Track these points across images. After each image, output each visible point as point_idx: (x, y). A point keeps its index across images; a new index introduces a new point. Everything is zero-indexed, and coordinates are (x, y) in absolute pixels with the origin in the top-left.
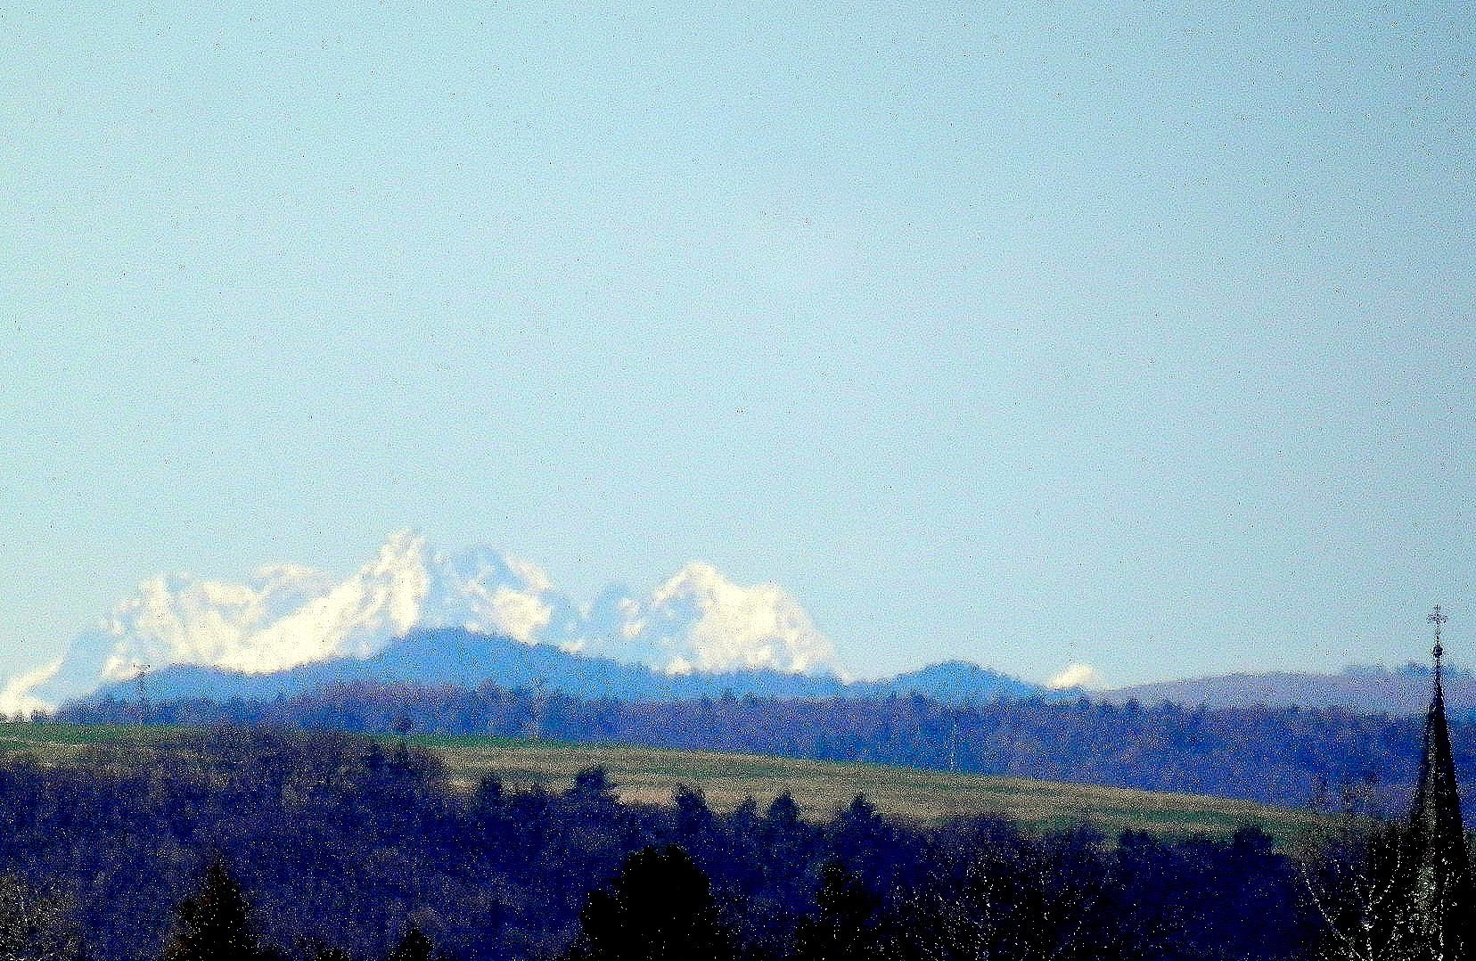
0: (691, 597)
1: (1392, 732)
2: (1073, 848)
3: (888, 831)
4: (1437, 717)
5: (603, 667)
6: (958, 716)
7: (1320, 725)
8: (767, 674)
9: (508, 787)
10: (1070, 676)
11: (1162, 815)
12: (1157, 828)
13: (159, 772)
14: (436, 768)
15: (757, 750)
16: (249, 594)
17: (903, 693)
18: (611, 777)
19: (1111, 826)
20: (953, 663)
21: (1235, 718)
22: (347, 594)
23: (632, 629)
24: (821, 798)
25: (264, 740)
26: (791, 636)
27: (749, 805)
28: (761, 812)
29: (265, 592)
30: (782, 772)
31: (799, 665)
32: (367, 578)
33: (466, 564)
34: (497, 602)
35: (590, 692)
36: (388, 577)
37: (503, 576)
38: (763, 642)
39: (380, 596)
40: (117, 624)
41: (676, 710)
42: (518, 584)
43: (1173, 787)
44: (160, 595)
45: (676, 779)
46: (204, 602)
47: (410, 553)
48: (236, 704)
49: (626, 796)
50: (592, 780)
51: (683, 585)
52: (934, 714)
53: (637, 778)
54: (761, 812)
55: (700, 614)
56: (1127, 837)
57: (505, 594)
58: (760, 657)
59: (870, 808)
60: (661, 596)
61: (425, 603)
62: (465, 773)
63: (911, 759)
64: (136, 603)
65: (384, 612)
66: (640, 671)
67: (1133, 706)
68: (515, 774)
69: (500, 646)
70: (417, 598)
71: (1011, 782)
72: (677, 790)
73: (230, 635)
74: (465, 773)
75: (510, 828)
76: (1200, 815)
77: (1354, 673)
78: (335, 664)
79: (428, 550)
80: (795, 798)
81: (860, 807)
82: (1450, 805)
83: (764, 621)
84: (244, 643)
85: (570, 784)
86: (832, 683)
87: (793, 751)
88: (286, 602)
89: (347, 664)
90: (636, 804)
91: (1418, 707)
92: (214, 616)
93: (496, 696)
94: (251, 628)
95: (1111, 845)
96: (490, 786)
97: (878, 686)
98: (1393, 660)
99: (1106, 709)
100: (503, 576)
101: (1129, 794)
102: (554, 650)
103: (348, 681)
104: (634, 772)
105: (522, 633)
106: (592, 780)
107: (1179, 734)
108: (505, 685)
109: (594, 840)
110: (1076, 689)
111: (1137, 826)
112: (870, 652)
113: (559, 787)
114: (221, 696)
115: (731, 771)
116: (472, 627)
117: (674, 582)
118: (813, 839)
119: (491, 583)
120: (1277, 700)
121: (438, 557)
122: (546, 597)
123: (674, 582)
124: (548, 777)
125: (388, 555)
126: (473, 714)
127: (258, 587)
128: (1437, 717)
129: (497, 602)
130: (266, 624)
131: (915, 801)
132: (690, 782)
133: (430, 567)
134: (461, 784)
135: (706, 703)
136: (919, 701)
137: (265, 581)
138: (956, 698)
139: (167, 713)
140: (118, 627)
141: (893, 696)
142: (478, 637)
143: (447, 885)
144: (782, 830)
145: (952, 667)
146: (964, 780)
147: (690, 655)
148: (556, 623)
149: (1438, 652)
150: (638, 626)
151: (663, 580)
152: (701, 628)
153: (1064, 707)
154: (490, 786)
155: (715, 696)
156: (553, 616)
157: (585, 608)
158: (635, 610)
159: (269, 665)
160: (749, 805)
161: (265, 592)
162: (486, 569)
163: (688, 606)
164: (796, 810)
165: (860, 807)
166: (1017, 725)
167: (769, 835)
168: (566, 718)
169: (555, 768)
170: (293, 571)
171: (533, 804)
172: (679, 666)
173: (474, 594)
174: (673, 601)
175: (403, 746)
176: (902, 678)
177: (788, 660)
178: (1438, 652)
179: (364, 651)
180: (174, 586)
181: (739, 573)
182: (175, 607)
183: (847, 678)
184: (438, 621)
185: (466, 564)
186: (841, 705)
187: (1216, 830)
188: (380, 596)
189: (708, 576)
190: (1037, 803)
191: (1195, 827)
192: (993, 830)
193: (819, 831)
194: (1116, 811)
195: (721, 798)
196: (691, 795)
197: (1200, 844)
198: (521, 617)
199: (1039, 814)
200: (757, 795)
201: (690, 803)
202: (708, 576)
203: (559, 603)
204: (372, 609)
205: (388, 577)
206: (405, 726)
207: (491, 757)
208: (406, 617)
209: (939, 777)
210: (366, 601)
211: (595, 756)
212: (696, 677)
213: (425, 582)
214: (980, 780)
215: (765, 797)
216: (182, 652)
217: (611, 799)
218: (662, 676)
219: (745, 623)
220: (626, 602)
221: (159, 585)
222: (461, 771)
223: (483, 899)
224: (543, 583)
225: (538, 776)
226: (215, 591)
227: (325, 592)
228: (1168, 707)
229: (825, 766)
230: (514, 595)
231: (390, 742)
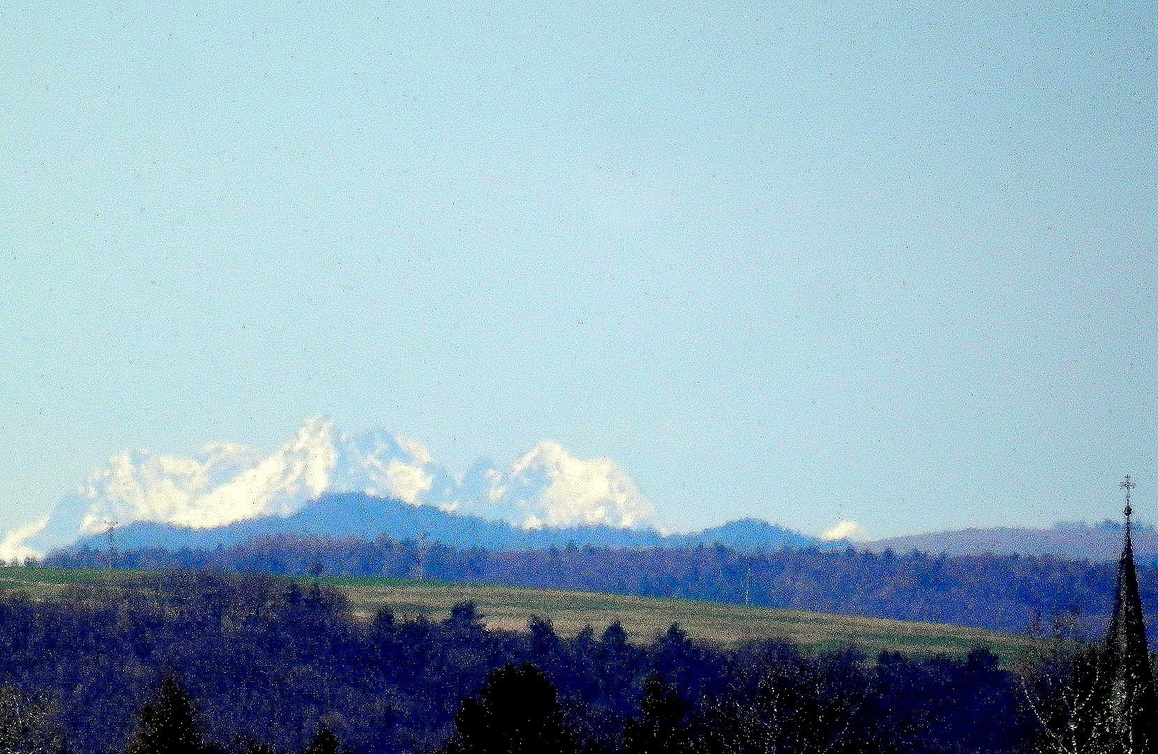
0: (542, 469)
1: (1092, 574)
2: (842, 665)
3: (696, 652)
4: (1127, 562)
5: (473, 524)
6: (752, 562)
7: (1036, 569)
8: (602, 529)
9: (399, 617)
10: (839, 530)
11: (912, 639)
12: (908, 649)
13: (124, 606)
14: (342, 603)
15: (594, 588)
16: (195, 466)
17: (709, 544)
18: (479, 610)
19: (871, 648)
20: (748, 520)
21: (969, 563)
22: (272, 466)
23: (496, 493)
24: (644, 626)
25: (207, 581)
26: (621, 499)
27: (588, 631)
28: (597, 637)
29: (208, 465)
30: (614, 606)
31: (627, 522)
32: (288, 453)
33: (366, 443)
34: (390, 472)
35: (463, 543)
36: (304, 453)
37: (395, 452)
38: (599, 504)
39: (298, 467)
40: (92, 490)
41: (531, 557)
42: (407, 458)
43: (920, 617)
44: (125, 467)
45: (531, 611)
46: (160, 472)
47: (322, 434)
48: (185, 552)
49: (491, 625)
50: (465, 612)
51: (536, 459)
52: (733, 560)
53: (500, 610)
54: (597, 637)
55: (549, 482)
56: (884, 657)
57: (397, 466)
58: (597, 516)
59: (683, 634)
60: (519, 467)
61: (334, 473)
62: (365, 607)
63: (715, 595)
64: (107, 473)
65: (301, 480)
66: (502, 527)
67: (889, 554)
68: (404, 607)
69: (392, 507)
70: (327, 469)
71: (793, 613)
72: (531, 620)
73: (181, 498)
74: (365, 607)
75: (400, 650)
76: (941, 640)
77: (1062, 528)
78: (262, 521)
79: (336, 432)
80: (624, 626)
81: (675, 633)
82: (1137, 632)
83: (599, 488)
84: (191, 504)
85: (447, 615)
86: (653, 536)
87: (622, 589)
88: (224, 473)
89: (272, 521)
90: (499, 631)
91: (1113, 554)
92: (168, 483)
93: (389, 546)
94: (197, 493)
95: (872, 663)
96: (385, 617)
97: (689, 538)
98: (1093, 518)
99: (868, 556)
100: (395, 452)
101: (886, 623)
102: (435, 510)
103: (273, 534)
104: (497, 606)
105: (410, 497)
106: (465, 612)
107: (925, 576)
108: (397, 538)
109: (466, 659)
110: (844, 541)
111: (892, 648)
112: (682, 512)
113: (438, 618)
114: (173, 546)
115: (573, 605)
116: (371, 492)
117: (529, 457)
118: (638, 658)
119: (385, 458)
120: (1002, 550)
121: (343, 437)
122: (429, 468)
123: (529, 457)
124: (430, 609)
125: (304, 435)
126: (371, 560)
127: (202, 461)
128: (1127, 562)
129: (390, 472)
130: (209, 490)
131: (718, 629)
132: (541, 614)
133: (338, 445)
134: (362, 615)
135: (554, 552)
136: (721, 550)
137: (208, 456)
138: (750, 548)
139: (131, 559)
140: (93, 492)
141: (701, 546)
142: (375, 500)
143: (351, 694)
144: (614, 652)
145: (747, 524)
146: (757, 612)
147: (542, 514)
148: (436, 489)
149: (1128, 511)
150: (501, 491)
151: (521, 455)
152: (550, 493)
153: (835, 555)
154: (385, 617)
155: (561, 546)
156: (434, 484)
157: (459, 477)
158: (498, 478)
159: (211, 522)
160: (588, 631)
161: (208, 465)
162: (382, 446)
163: (540, 476)
164: (624, 635)
165: (675, 633)
166: (798, 569)
167: (603, 655)
168: (444, 564)
169: (436, 602)
170: (230, 448)
171: (418, 631)
172: (533, 523)
173: (372, 466)
174: (528, 472)
175: (316, 585)
176: (707, 532)
177: (618, 518)
178: (1128, 511)
179: (286, 511)
180: (136, 460)
181: (580, 450)
182: (137, 476)
183: (665, 532)
184: (344, 488)
185: (366, 443)
186: (659, 553)
187: (954, 651)
188: (298, 467)
189: (555, 452)
190: (813, 630)
191: (937, 649)
192: (779, 651)
193: (642, 652)
194: (876, 636)
195: (566, 626)
196: (542, 624)
197: (941, 662)
198: (409, 484)
199: (816, 638)
200: (594, 624)
201: (541, 630)
202: (555, 452)
203: (439, 473)
204: (292, 478)
205: (304, 453)
206: (318, 570)
207: (385, 594)
208: (319, 484)
209: (737, 610)
210: (287, 472)
211: (467, 593)
212: (546, 531)
213: (334, 456)
214: (769, 612)
215: (600, 625)
216: (142, 512)
217: (480, 627)
218: (519, 531)
219: (584, 489)
220: (491, 472)
221: (125, 459)
222: (362, 605)
223: (379, 705)
224: (426, 457)
225: (422, 609)
226: (169, 463)
227: (255, 465)
228: (917, 555)
229: (647, 601)
230: (403, 467)
231: (306, 582)
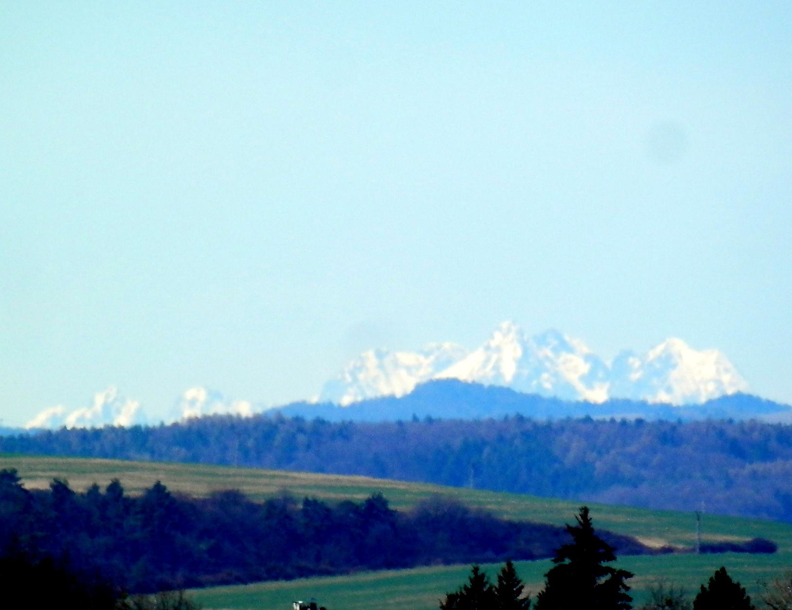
7: (743, 431)
11: (332, 488)
12: (321, 496)
16: (422, 358)
18: (19, 474)
19: (300, 493)
23: (635, 376)
24: (136, 483)
27: (95, 488)
28: (102, 491)
29: (432, 358)
30: (112, 469)
32: (488, 348)
33: (541, 340)
36: (498, 349)
37: (564, 346)
39: (494, 357)
40: (348, 376)
41: (11, 439)
42: (571, 350)
44: (372, 360)
46: (396, 364)
52: (529, 426)
53: (40, 473)
54: (102, 491)
55: (674, 366)
56: (307, 502)
57: (564, 356)
59: (164, 488)
65: (496, 367)
72: (52, 481)
79: (521, 333)
92: (403, 372)
95: (300, 506)
100: (564, 346)
115: (82, 472)
117: (660, 348)
118: (129, 504)
121: (525, 337)
122: (587, 358)
123: (660, 348)
125: (498, 335)
127: (427, 355)
129: (562, 359)
131: (192, 483)
132: (62, 476)
140: (349, 379)
145: (742, 400)
147: (669, 390)
151: (653, 347)
152: (674, 374)
157: (609, 363)
158: (637, 364)
160: (95, 488)
161: (432, 358)
162: (555, 342)
163: (668, 361)
164: (121, 490)
173: (547, 358)
180: (380, 355)
182: (381, 367)
185: (541, 340)
187: (360, 497)
188: (494, 357)
189: (679, 345)
191: (348, 496)
192: (231, 499)
195: (78, 485)
196: (59, 483)
197: (348, 505)
202: (679, 345)
205: (498, 349)
210: (487, 360)
211: (116, 475)
213: (519, 353)
215: (104, 483)
220: (631, 360)
221: (371, 354)
224: (585, 350)
229: (192, 467)
230: (570, 356)
